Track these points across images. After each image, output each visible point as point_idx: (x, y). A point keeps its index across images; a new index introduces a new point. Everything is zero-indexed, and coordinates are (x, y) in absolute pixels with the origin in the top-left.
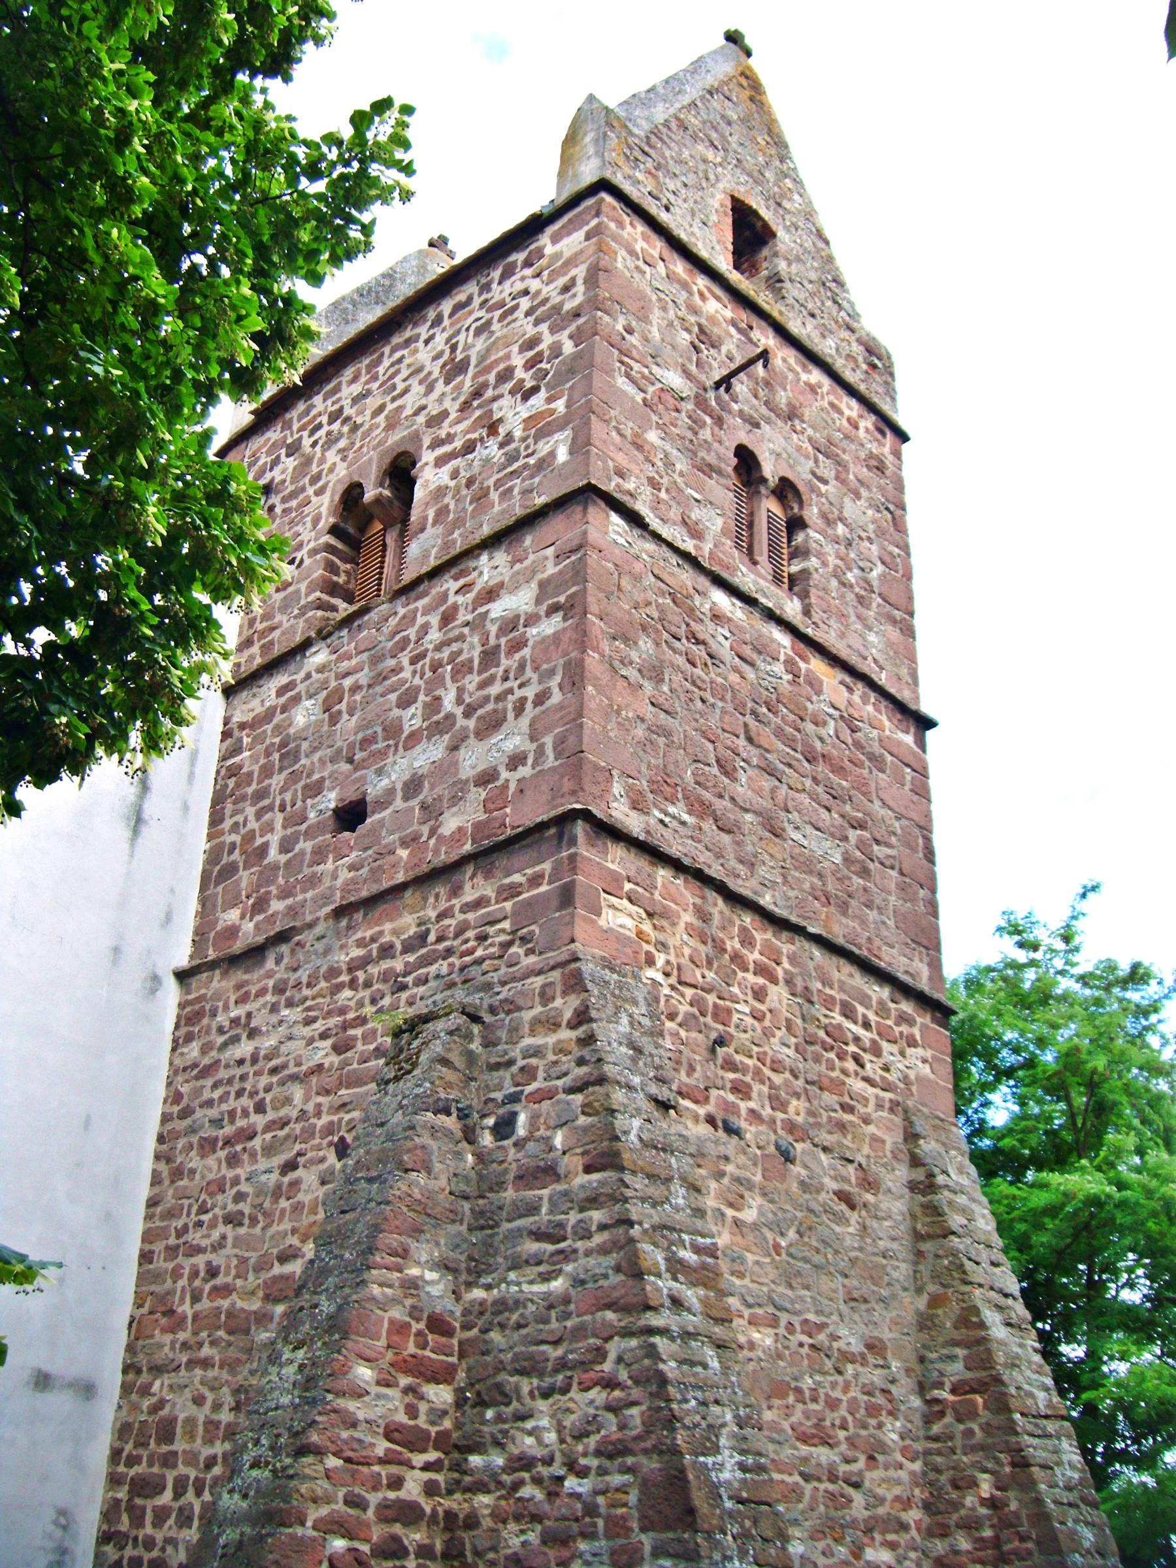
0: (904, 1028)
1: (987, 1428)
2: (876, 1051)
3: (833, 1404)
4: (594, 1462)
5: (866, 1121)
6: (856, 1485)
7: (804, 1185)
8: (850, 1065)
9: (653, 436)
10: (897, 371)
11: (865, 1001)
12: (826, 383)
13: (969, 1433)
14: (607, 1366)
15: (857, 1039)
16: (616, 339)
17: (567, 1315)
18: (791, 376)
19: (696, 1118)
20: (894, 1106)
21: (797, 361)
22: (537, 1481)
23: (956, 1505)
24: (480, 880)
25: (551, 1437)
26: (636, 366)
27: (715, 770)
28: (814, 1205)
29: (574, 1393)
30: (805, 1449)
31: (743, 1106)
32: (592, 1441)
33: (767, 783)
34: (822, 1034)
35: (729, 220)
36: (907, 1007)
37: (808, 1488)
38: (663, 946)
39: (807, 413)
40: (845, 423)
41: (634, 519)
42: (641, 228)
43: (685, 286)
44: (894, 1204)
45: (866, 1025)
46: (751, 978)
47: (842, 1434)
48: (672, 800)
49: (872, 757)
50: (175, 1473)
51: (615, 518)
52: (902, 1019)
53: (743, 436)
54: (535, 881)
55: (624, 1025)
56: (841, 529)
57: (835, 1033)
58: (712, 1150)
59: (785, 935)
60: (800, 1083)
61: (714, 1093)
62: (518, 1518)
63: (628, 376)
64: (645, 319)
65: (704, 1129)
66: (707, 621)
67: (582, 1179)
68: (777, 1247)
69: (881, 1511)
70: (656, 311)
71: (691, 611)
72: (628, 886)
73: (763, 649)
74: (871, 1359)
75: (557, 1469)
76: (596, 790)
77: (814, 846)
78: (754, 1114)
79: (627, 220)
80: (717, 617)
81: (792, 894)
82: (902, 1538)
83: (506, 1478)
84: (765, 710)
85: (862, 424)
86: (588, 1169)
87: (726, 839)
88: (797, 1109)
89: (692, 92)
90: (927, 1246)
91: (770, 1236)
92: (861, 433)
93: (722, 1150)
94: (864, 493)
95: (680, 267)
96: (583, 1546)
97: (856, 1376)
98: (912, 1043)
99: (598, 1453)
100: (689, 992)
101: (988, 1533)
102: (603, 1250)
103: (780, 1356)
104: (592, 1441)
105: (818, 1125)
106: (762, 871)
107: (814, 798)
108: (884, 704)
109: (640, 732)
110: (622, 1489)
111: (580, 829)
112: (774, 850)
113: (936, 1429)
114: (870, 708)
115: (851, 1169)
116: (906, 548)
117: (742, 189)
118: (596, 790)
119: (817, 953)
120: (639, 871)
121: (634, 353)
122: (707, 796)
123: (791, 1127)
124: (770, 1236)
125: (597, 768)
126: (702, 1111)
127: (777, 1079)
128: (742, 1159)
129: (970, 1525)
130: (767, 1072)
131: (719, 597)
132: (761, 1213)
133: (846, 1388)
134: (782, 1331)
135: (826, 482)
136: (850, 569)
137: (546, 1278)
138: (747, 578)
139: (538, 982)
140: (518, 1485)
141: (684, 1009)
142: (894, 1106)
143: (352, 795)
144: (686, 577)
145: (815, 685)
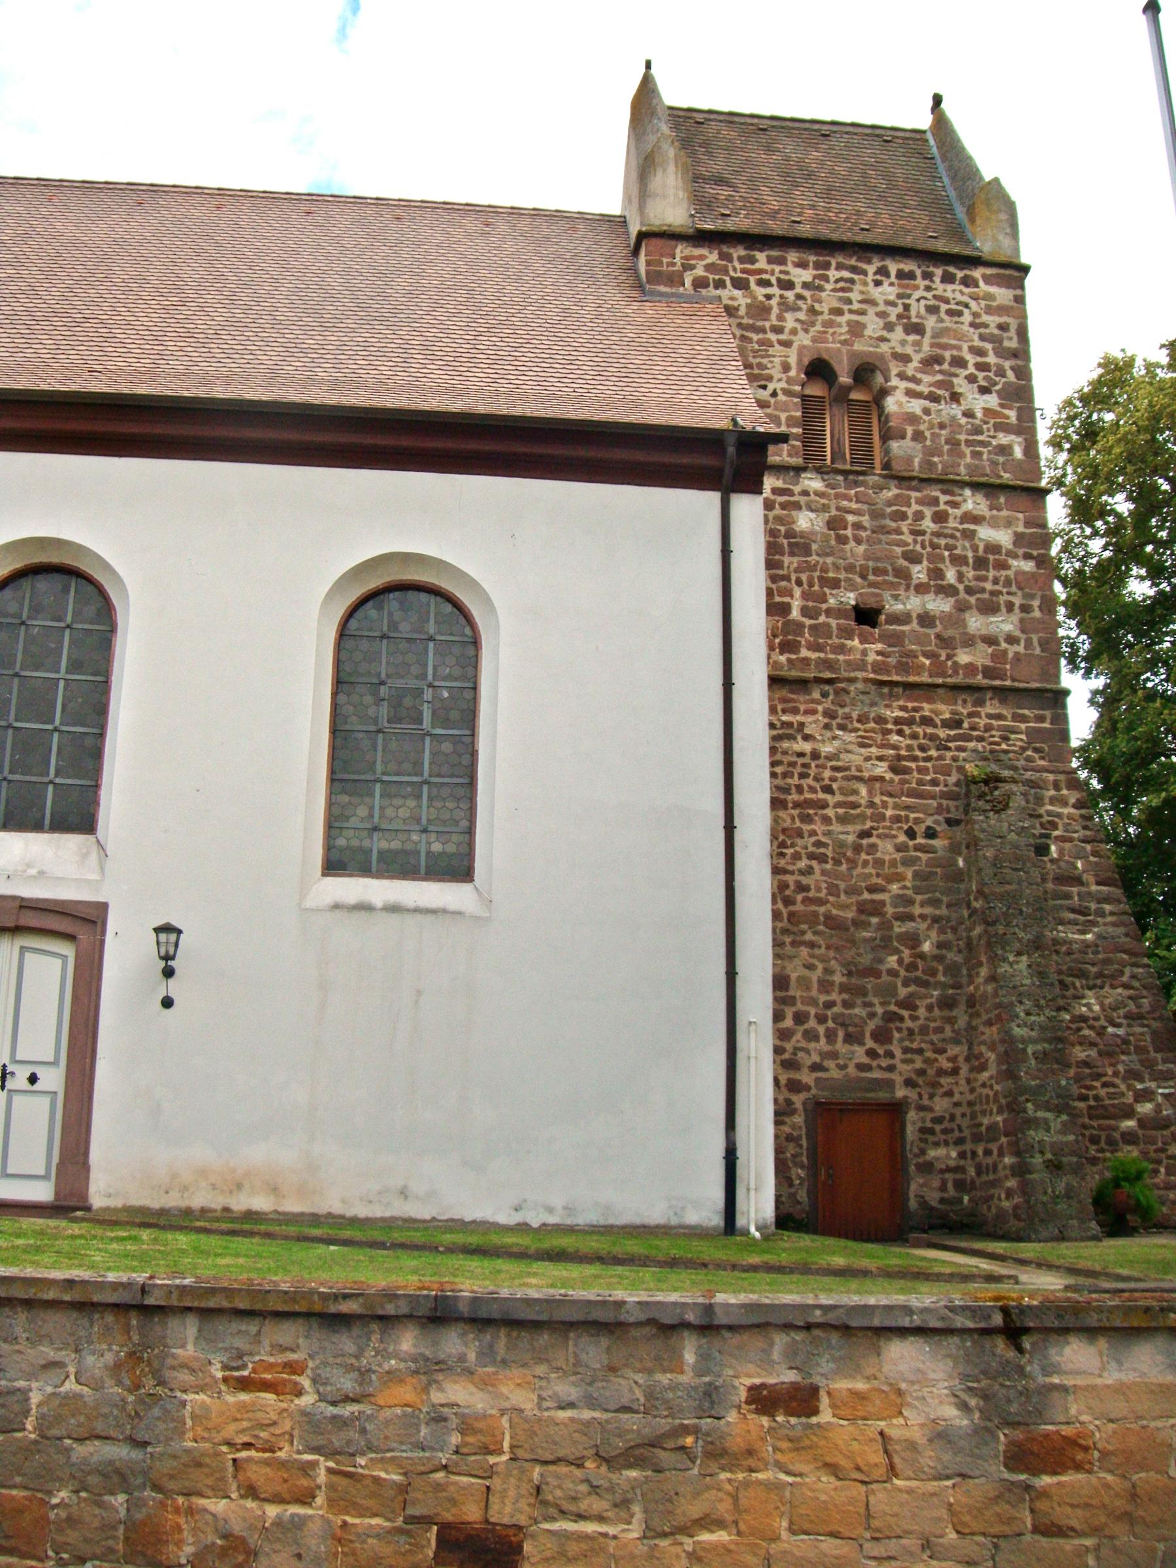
4: (1124, 1022)
14: (1125, 979)
17: (1097, 953)
22: (1091, 1028)
24: (996, 702)
25: (1097, 1008)
29: (1106, 989)
32: (1121, 1012)
50: (794, 1009)
54: (1041, 719)
62: (1081, 1044)
67: (1094, 888)
75: (1103, 1022)
83: (1073, 1026)
86: (1098, 883)
96: (1123, 1057)
99: (1126, 1017)
102: (1114, 924)
104: (1121, 1012)
110: (1142, 1034)
137: (1084, 932)
140: (1079, 1029)
143: (872, 603)
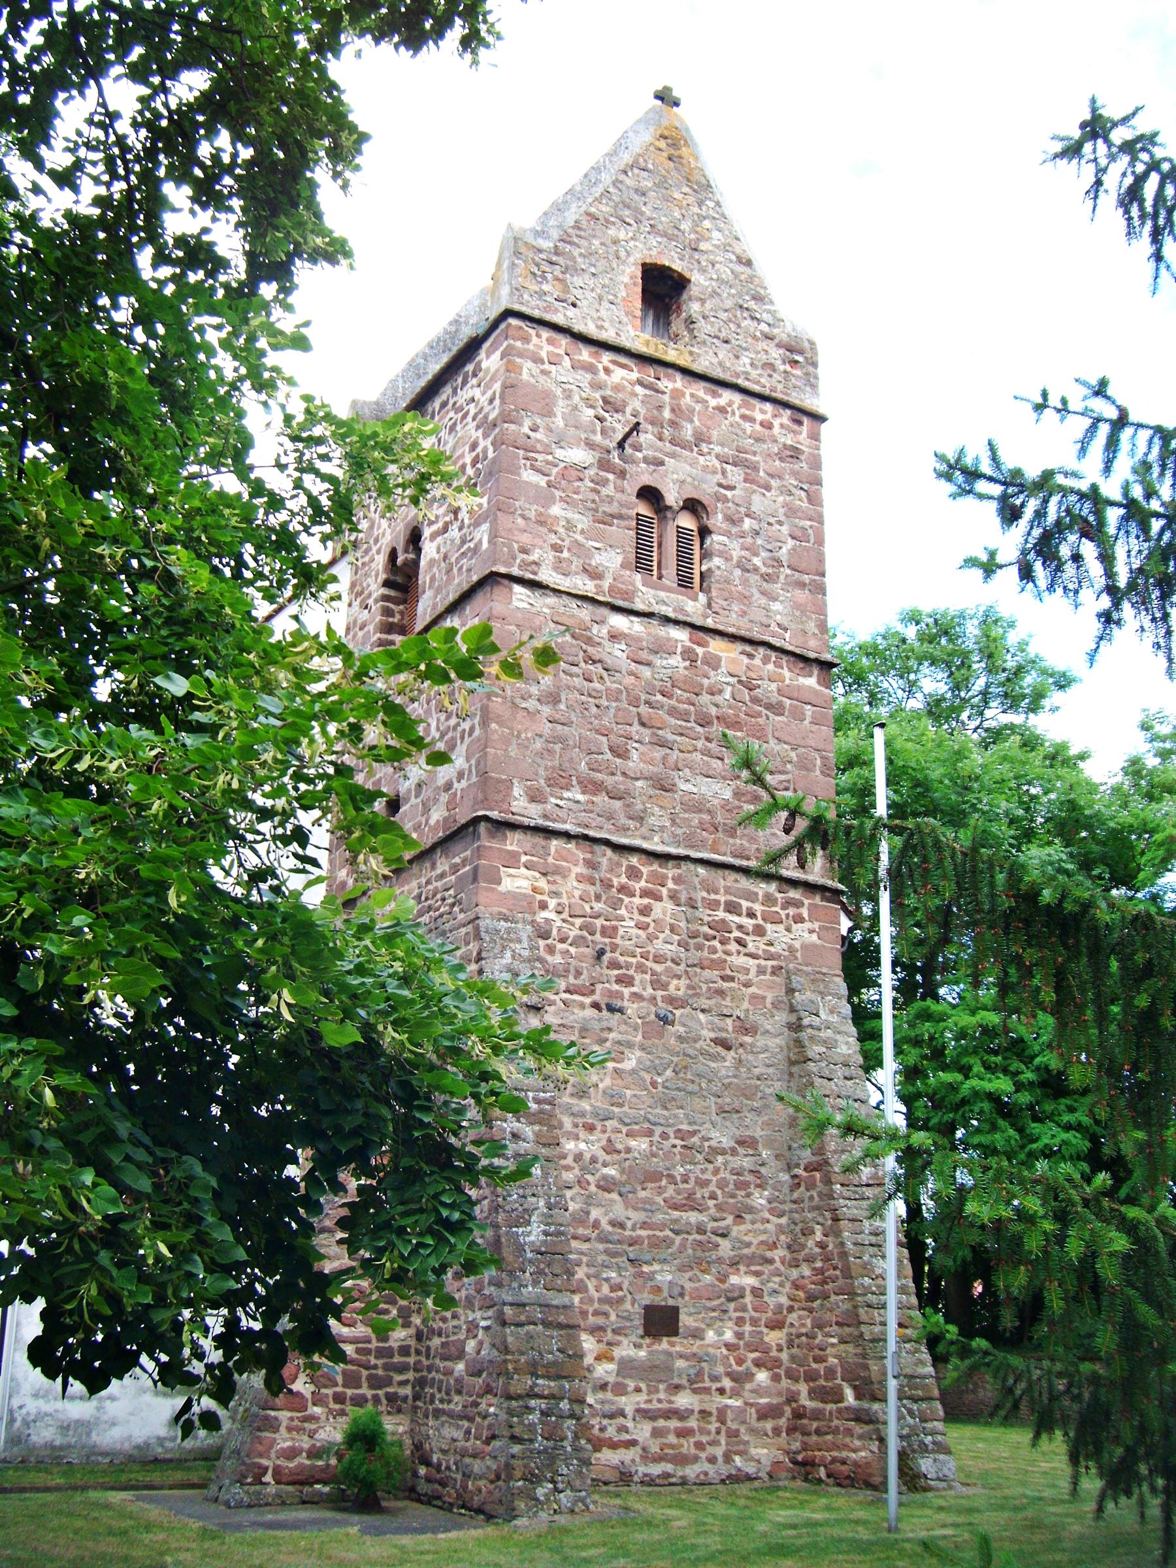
0: (791, 911)
1: (820, 1194)
2: (759, 931)
3: (704, 1184)
5: (747, 985)
6: (723, 1236)
7: (680, 1038)
8: (733, 947)
9: (556, 510)
10: (821, 360)
11: (751, 897)
12: (737, 398)
13: (811, 1198)
15: (740, 927)
16: (522, 441)
18: (698, 407)
19: (582, 1006)
20: (776, 971)
21: (707, 391)
23: (803, 1246)
26: (540, 457)
27: (609, 756)
28: (691, 1052)
30: (676, 1214)
31: (626, 991)
33: (658, 753)
34: (706, 929)
35: (639, 289)
36: (794, 894)
37: (678, 1240)
38: (556, 894)
39: (715, 434)
40: (758, 427)
41: (534, 585)
42: (546, 334)
43: (590, 369)
44: (772, 1040)
45: (751, 915)
46: (637, 901)
47: (711, 1203)
48: (567, 788)
49: (769, 707)
51: (517, 588)
52: (788, 903)
53: (646, 480)
55: (508, 957)
56: (748, 523)
57: (721, 927)
58: (596, 1026)
59: (671, 864)
60: (682, 967)
61: (599, 987)
63: (533, 468)
64: (550, 414)
65: (590, 1012)
66: (606, 643)
68: (654, 1084)
69: (746, 1251)
70: (561, 403)
71: (589, 641)
72: (524, 858)
73: (662, 648)
74: (741, 1150)
76: (498, 797)
77: (704, 790)
78: (636, 996)
79: (532, 332)
80: (614, 637)
81: (679, 831)
82: (767, 1269)
84: (659, 697)
85: (776, 423)
87: (618, 804)
88: (678, 987)
89: (606, 178)
90: (795, 1069)
91: (647, 1077)
92: (776, 430)
93: (605, 1024)
94: (774, 483)
95: (585, 354)
97: (726, 1164)
98: (799, 919)
100: (578, 922)
101: (819, 1264)
103: (654, 1155)
105: (697, 995)
106: (652, 820)
107: (707, 753)
108: (784, 660)
109: (538, 745)
111: (482, 827)
112: (665, 803)
113: (796, 1195)
114: (771, 667)
115: (729, 1021)
116: (820, 519)
117: (654, 252)
118: (498, 797)
119: (701, 870)
120: (534, 846)
121: (539, 447)
122: (599, 776)
123: (671, 1000)
124: (647, 1077)
125: (499, 781)
126: (588, 1000)
127: (659, 968)
128: (623, 1028)
129: (809, 1260)
130: (649, 964)
131: (619, 622)
132: (639, 1061)
133: (716, 1171)
134: (656, 1138)
135: (732, 488)
136: (756, 554)
138: (646, 597)
139: (463, 930)
141: (573, 933)
142: (776, 971)
144: (585, 613)
145: (713, 662)
